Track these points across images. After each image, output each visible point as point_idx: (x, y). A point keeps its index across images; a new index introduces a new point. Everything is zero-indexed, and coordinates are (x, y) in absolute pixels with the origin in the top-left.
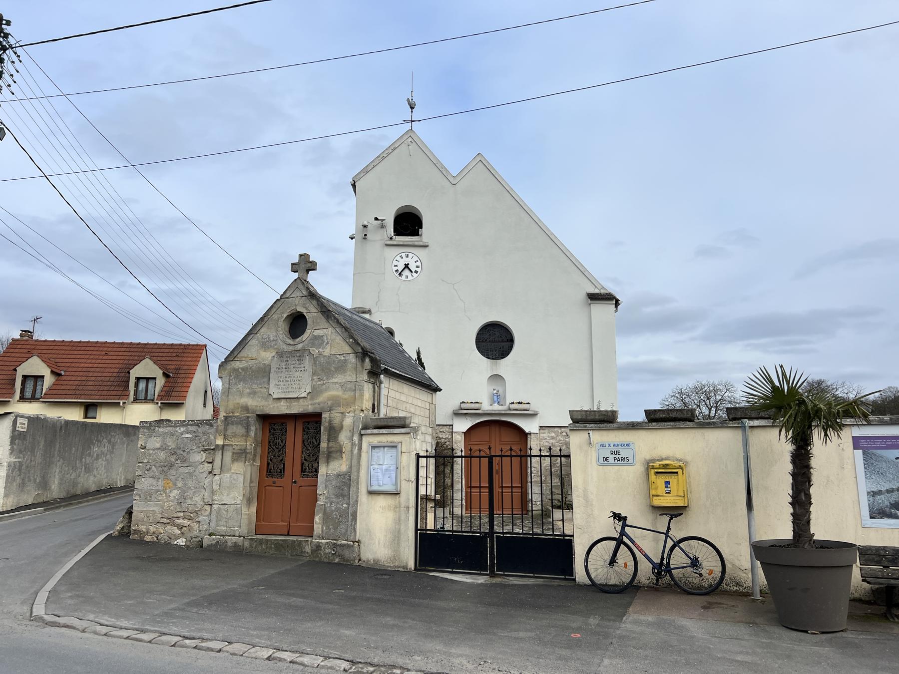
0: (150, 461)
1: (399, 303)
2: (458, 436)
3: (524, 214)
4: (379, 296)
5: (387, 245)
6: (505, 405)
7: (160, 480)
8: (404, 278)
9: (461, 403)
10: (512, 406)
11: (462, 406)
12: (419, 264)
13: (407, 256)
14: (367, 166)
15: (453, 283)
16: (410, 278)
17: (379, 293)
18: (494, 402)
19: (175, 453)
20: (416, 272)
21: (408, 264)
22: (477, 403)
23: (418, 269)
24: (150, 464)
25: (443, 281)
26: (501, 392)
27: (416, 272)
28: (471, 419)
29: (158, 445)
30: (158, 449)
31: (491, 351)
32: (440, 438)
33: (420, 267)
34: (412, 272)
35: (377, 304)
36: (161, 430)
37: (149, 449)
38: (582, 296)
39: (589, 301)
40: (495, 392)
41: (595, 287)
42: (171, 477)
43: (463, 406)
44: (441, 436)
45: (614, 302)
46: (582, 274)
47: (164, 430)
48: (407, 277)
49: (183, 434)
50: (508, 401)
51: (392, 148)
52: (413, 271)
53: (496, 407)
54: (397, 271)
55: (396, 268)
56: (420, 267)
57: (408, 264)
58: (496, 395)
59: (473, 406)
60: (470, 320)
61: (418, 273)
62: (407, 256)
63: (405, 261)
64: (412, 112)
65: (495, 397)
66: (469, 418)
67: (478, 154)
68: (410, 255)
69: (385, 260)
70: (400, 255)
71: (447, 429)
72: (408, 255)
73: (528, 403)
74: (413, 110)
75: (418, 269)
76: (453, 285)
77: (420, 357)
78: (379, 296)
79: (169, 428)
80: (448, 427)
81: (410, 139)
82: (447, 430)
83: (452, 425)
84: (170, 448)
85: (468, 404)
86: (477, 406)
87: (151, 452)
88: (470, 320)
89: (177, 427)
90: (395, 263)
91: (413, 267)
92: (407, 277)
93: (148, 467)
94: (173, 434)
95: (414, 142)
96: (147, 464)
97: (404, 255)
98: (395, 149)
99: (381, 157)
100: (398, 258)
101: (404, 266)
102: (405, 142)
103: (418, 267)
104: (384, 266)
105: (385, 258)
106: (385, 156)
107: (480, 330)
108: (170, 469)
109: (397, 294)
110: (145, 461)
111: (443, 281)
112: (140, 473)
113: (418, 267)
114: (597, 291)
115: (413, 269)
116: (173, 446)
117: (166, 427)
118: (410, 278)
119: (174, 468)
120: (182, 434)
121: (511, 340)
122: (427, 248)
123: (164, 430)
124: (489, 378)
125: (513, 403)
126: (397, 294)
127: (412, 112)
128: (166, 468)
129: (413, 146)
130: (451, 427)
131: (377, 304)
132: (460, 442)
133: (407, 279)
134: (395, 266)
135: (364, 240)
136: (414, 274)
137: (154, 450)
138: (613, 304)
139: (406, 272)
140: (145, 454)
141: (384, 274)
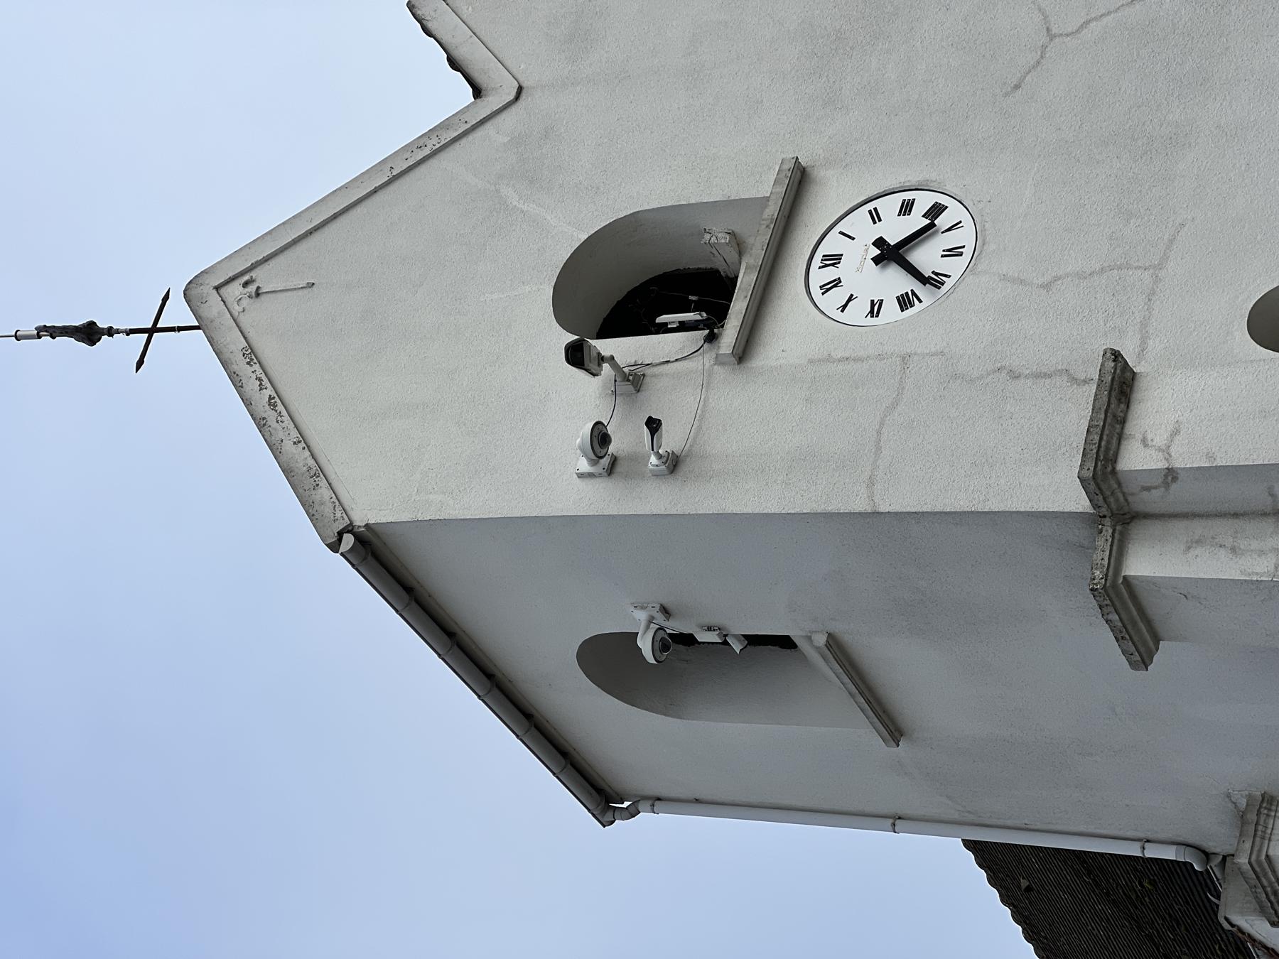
1: (1102, 270)
4: (1038, 376)
8: (954, 267)
15: (1045, 40)
16: (965, 237)
51: (240, 364)
54: (905, 302)
69: (829, 359)
74: (102, 324)
78: (1038, 376)
90: (857, 313)
91: (896, 229)
95: (254, 274)
97: (820, 276)
98: (251, 354)
102: (236, 309)
104: (856, 360)
105: (811, 361)
106: (269, 391)
109: (1046, 287)
139: (926, 257)
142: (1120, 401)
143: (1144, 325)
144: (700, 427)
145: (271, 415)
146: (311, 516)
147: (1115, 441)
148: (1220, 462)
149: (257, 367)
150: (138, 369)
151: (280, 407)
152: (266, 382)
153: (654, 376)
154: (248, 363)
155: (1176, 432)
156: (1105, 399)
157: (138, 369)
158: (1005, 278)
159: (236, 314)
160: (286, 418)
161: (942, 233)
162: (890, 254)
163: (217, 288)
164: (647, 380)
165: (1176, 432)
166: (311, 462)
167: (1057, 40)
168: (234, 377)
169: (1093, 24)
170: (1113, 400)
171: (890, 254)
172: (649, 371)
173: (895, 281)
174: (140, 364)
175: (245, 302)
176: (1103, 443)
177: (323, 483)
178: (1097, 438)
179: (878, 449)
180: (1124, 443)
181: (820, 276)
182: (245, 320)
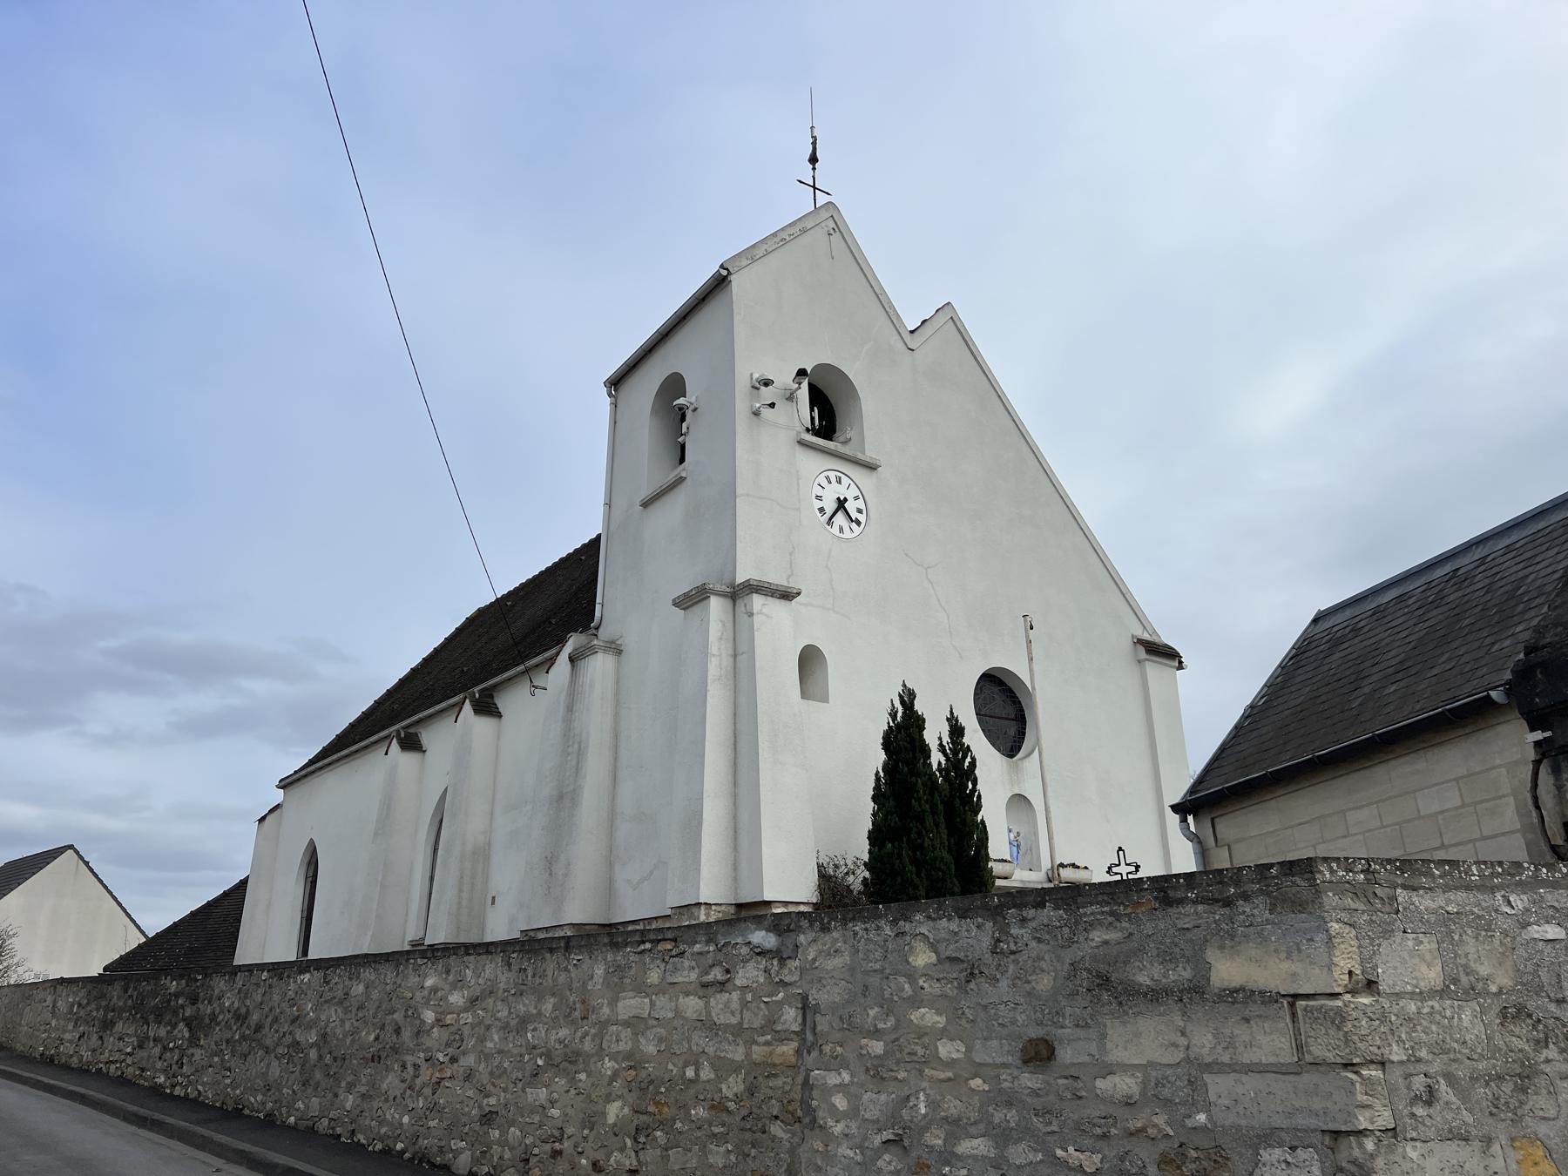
0: (1423, 1054)
1: (833, 589)
3: (1025, 448)
5: (801, 443)
7: (1496, 1148)
8: (835, 530)
14: (754, 246)
16: (847, 534)
17: (791, 554)
19: (1521, 1013)
20: (858, 523)
24: (1422, 1068)
29: (1432, 975)
30: (1433, 993)
36: (1424, 902)
37: (1399, 996)
42: (1543, 1129)
46: (1121, 596)
47: (1441, 901)
48: (841, 530)
49: (1528, 924)
54: (821, 510)
55: (818, 504)
57: (846, 500)
60: (961, 657)
63: (838, 493)
64: (814, 169)
69: (798, 479)
70: (860, 496)
79: (1461, 896)
84: (1493, 989)
87: (1412, 1007)
89: (1493, 890)
93: (1419, 1083)
94: (1489, 923)
95: (838, 233)
96: (1411, 1068)
101: (835, 506)
102: (823, 225)
104: (798, 490)
108: (1524, 1090)
109: (827, 567)
110: (1397, 1054)
112: (1385, 1119)
116: (1503, 979)
117: (1447, 889)
119: (1541, 1081)
120: (1525, 925)
123: (1441, 901)
124: (1010, 799)
127: (814, 169)
128: (1507, 1088)
129: (836, 237)
135: (755, 418)
136: (854, 525)
137: (1421, 996)
140: (1383, 1018)
148: (756, 633)
149: (799, 233)
151: (781, 243)
152: (792, 237)
153: (792, 406)
155: (768, 617)
160: (777, 246)
162: (841, 504)
163: (832, 216)
165: (768, 617)
166: (758, 257)
167: (924, 571)
171: (841, 504)
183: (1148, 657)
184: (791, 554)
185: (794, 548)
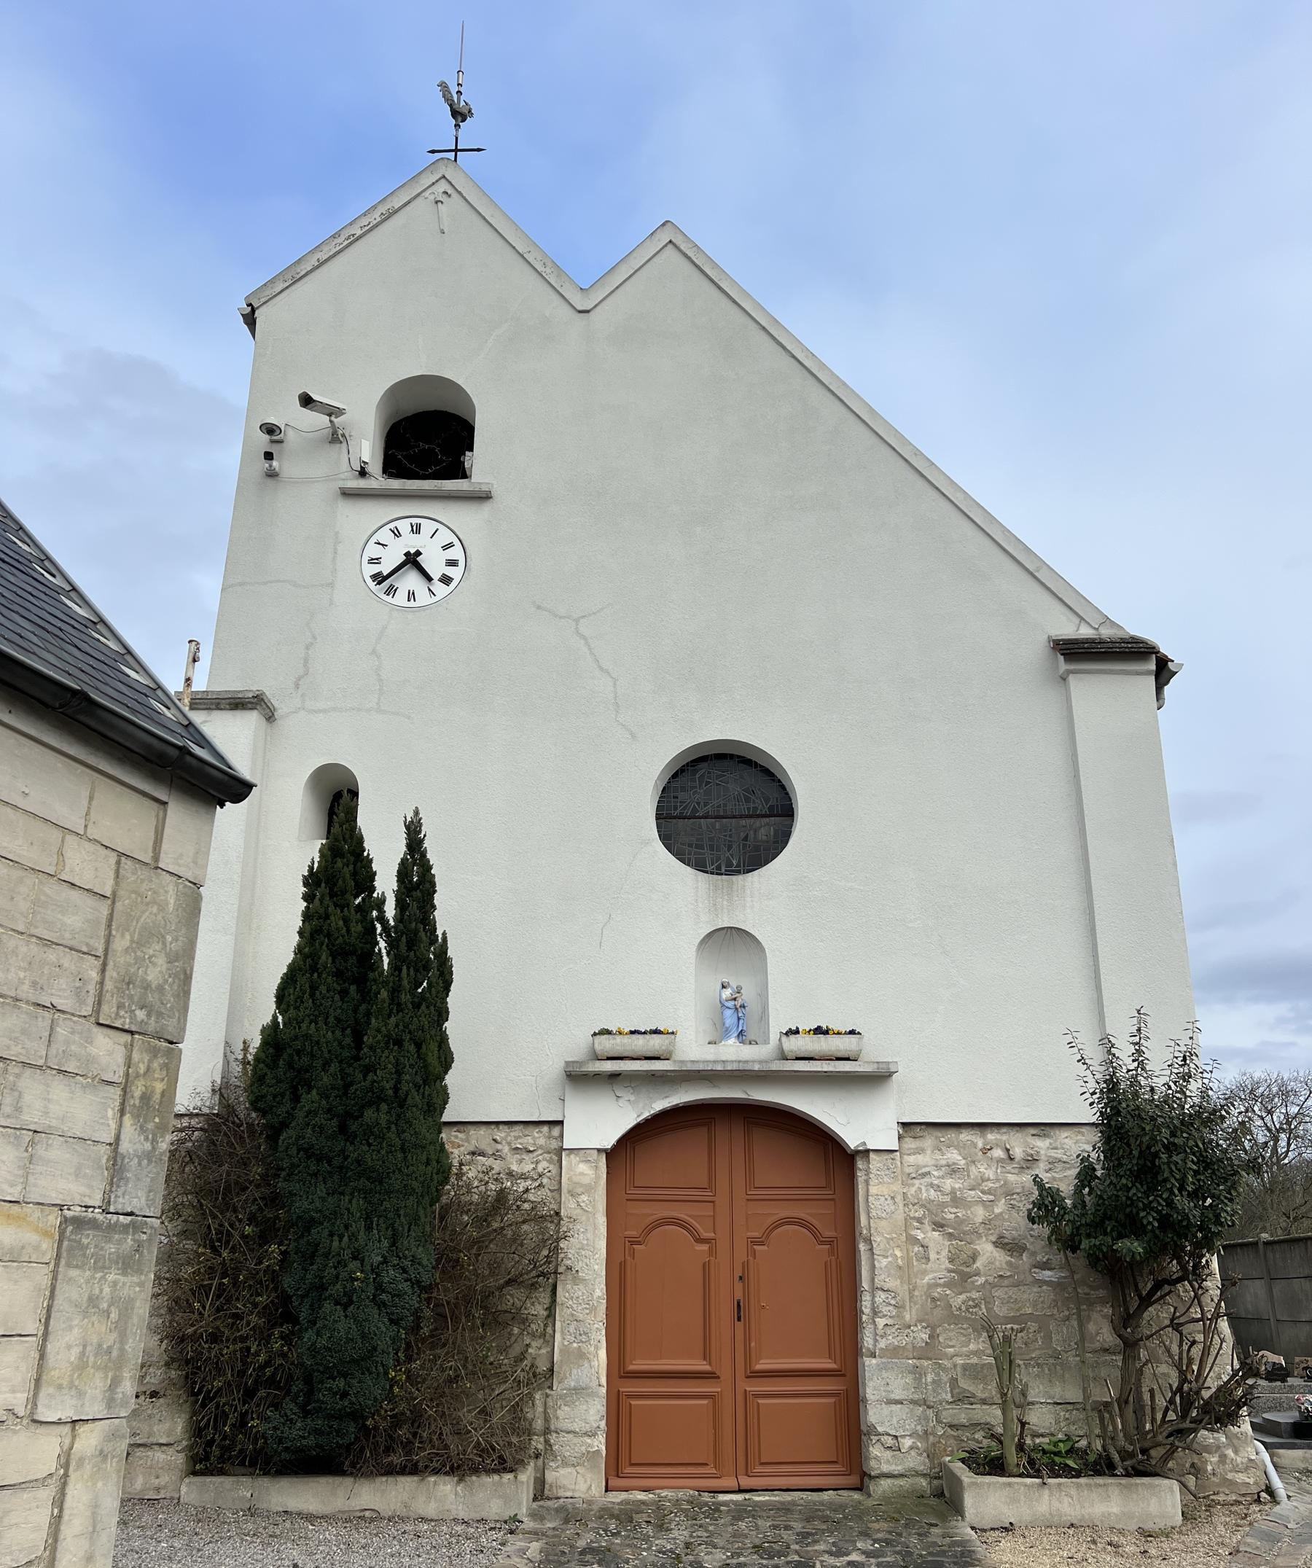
2: (583, 1167)
3: (816, 394)
4: (306, 661)
5: (347, 494)
6: (766, 1042)
8: (400, 598)
9: (595, 1034)
10: (792, 1044)
11: (596, 1046)
12: (456, 553)
13: (416, 530)
17: (307, 648)
18: (725, 1033)
20: (446, 580)
21: (418, 553)
22: (656, 1032)
23: (450, 571)
25: (539, 607)
26: (748, 996)
27: (446, 580)
28: (632, 1098)
31: (712, 848)
32: (510, 1174)
33: (462, 563)
34: (429, 579)
35: (297, 686)
38: (1034, 649)
39: (1063, 665)
40: (727, 993)
41: (1077, 620)
43: (605, 1044)
44: (514, 1167)
45: (1153, 667)
48: (411, 596)
50: (777, 1025)
51: (383, 209)
52: (436, 576)
53: (732, 1052)
56: (462, 563)
57: (418, 553)
58: (731, 1004)
59: (639, 1044)
60: (633, 736)
61: (453, 585)
62: (416, 530)
65: (728, 1013)
66: (627, 1095)
67: (664, 225)
68: (428, 527)
70: (392, 526)
71: (538, 1138)
72: (419, 526)
73: (852, 1032)
75: (450, 571)
76: (577, 621)
77: (422, 841)
78: (306, 661)
80: (545, 1129)
81: (443, 186)
82: (542, 1141)
83: (561, 1123)
85: (619, 1039)
86: (655, 1043)
88: (633, 736)
90: (372, 551)
92: (411, 596)
95: (455, 195)
97: (404, 526)
99: (343, 237)
100: (384, 535)
102: (426, 194)
103: (452, 563)
104: (334, 559)
105: (337, 533)
106: (359, 232)
107: (675, 776)
109: (374, 652)
111: (539, 607)
113: (452, 563)
114: (1085, 632)
115: (435, 569)
118: (423, 598)
121: (783, 810)
122: (486, 508)
125: (797, 1032)
126: (374, 652)
130: (556, 1131)
131: (297, 686)
132: (589, 1189)
133: (412, 604)
134: (373, 561)
135: (269, 481)
136: (440, 589)
138: (1148, 673)
139: (410, 580)
141: (331, 585)
142: (230, 704)
143: (334, 709)
144: (314, 482)
145: (343, 237)
146: (265, 285)
147: (205, 706)
149: (379, 219)
150: (429, 152)
151: (346, 242)
154: (382, 214)
156: (226, 697)
157: (429, 152)
158: (385, 628)
159: (423, 194)
160: (338, 248)
161: (430, 590)
162: (412, 560)
164: (338, 445)
166: (303, 273)
167: (574, 623)
168: (374, 207)
169: (583, 642)
170: (228, 701)
171: (412, 560)
172: (345, 443)
173: (392, 559)
174: (479, 150)
175: (432, 197)
176: (197, 701)
177: (287, 284)
178: (199, 697)
179: (265, 583)
180: (205, 712)
181: (404, 526)
182: (420, 200)
183: (1072, 667)
184: (307, 648)
185: (314, 637)
